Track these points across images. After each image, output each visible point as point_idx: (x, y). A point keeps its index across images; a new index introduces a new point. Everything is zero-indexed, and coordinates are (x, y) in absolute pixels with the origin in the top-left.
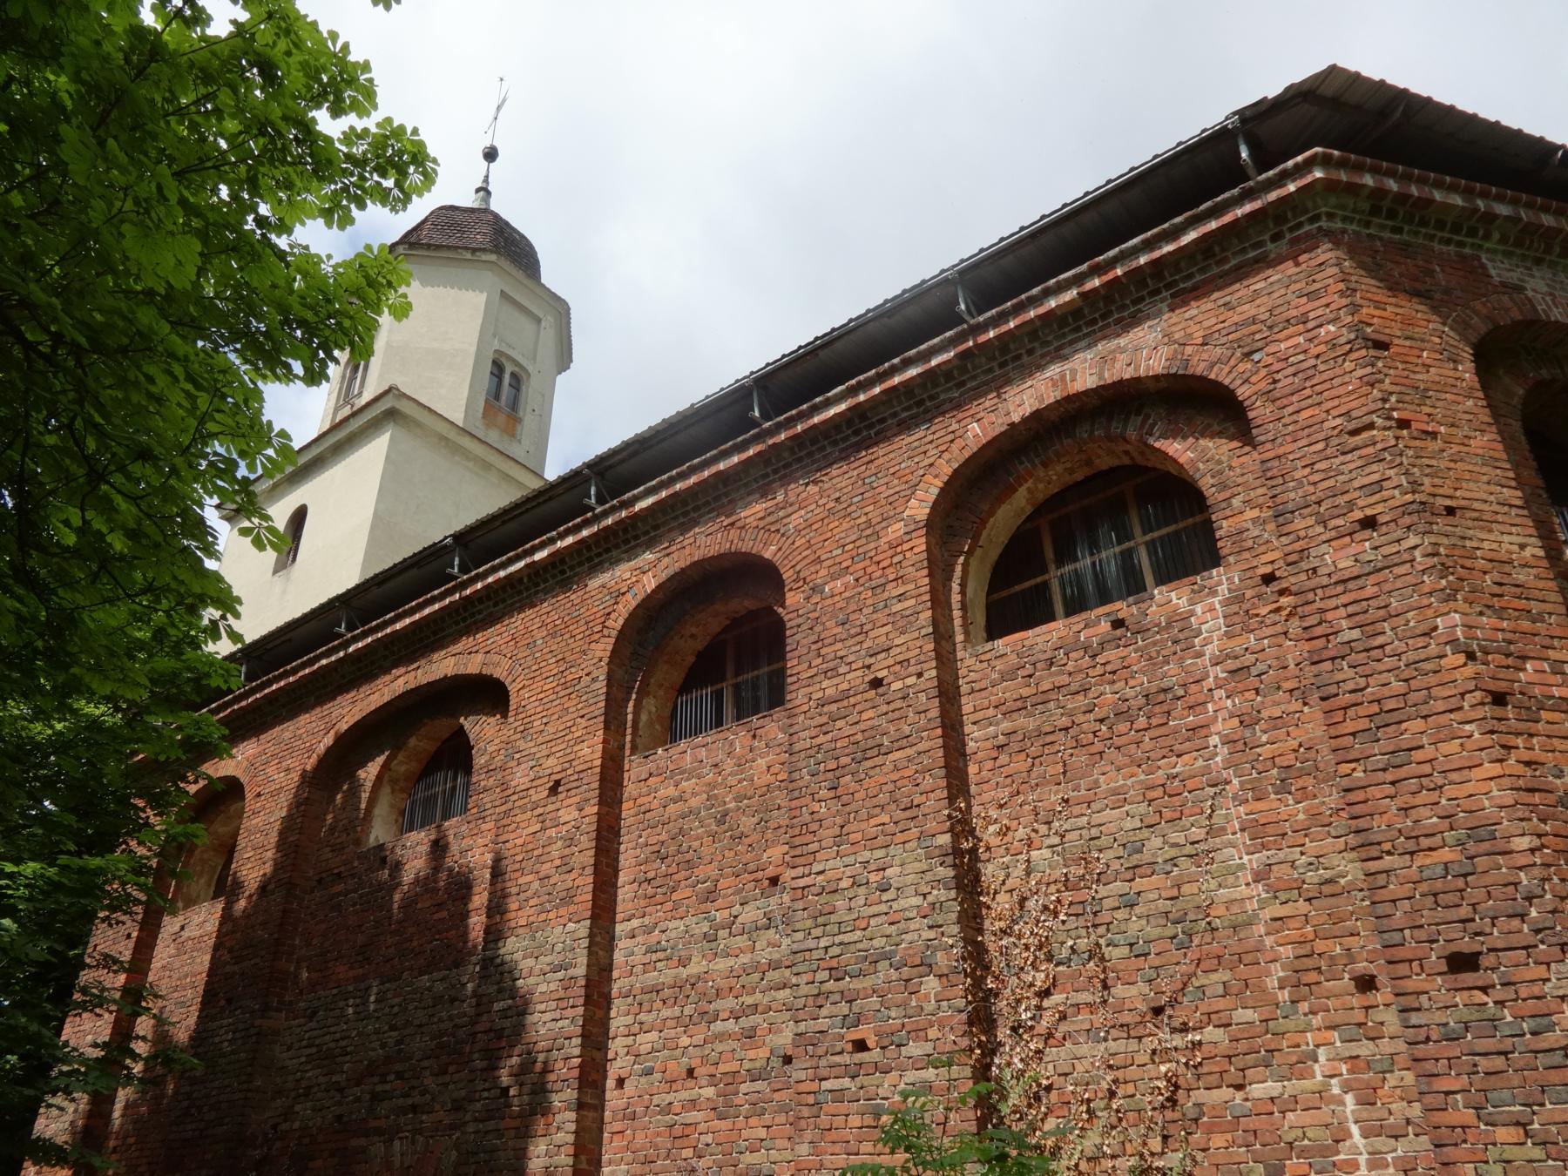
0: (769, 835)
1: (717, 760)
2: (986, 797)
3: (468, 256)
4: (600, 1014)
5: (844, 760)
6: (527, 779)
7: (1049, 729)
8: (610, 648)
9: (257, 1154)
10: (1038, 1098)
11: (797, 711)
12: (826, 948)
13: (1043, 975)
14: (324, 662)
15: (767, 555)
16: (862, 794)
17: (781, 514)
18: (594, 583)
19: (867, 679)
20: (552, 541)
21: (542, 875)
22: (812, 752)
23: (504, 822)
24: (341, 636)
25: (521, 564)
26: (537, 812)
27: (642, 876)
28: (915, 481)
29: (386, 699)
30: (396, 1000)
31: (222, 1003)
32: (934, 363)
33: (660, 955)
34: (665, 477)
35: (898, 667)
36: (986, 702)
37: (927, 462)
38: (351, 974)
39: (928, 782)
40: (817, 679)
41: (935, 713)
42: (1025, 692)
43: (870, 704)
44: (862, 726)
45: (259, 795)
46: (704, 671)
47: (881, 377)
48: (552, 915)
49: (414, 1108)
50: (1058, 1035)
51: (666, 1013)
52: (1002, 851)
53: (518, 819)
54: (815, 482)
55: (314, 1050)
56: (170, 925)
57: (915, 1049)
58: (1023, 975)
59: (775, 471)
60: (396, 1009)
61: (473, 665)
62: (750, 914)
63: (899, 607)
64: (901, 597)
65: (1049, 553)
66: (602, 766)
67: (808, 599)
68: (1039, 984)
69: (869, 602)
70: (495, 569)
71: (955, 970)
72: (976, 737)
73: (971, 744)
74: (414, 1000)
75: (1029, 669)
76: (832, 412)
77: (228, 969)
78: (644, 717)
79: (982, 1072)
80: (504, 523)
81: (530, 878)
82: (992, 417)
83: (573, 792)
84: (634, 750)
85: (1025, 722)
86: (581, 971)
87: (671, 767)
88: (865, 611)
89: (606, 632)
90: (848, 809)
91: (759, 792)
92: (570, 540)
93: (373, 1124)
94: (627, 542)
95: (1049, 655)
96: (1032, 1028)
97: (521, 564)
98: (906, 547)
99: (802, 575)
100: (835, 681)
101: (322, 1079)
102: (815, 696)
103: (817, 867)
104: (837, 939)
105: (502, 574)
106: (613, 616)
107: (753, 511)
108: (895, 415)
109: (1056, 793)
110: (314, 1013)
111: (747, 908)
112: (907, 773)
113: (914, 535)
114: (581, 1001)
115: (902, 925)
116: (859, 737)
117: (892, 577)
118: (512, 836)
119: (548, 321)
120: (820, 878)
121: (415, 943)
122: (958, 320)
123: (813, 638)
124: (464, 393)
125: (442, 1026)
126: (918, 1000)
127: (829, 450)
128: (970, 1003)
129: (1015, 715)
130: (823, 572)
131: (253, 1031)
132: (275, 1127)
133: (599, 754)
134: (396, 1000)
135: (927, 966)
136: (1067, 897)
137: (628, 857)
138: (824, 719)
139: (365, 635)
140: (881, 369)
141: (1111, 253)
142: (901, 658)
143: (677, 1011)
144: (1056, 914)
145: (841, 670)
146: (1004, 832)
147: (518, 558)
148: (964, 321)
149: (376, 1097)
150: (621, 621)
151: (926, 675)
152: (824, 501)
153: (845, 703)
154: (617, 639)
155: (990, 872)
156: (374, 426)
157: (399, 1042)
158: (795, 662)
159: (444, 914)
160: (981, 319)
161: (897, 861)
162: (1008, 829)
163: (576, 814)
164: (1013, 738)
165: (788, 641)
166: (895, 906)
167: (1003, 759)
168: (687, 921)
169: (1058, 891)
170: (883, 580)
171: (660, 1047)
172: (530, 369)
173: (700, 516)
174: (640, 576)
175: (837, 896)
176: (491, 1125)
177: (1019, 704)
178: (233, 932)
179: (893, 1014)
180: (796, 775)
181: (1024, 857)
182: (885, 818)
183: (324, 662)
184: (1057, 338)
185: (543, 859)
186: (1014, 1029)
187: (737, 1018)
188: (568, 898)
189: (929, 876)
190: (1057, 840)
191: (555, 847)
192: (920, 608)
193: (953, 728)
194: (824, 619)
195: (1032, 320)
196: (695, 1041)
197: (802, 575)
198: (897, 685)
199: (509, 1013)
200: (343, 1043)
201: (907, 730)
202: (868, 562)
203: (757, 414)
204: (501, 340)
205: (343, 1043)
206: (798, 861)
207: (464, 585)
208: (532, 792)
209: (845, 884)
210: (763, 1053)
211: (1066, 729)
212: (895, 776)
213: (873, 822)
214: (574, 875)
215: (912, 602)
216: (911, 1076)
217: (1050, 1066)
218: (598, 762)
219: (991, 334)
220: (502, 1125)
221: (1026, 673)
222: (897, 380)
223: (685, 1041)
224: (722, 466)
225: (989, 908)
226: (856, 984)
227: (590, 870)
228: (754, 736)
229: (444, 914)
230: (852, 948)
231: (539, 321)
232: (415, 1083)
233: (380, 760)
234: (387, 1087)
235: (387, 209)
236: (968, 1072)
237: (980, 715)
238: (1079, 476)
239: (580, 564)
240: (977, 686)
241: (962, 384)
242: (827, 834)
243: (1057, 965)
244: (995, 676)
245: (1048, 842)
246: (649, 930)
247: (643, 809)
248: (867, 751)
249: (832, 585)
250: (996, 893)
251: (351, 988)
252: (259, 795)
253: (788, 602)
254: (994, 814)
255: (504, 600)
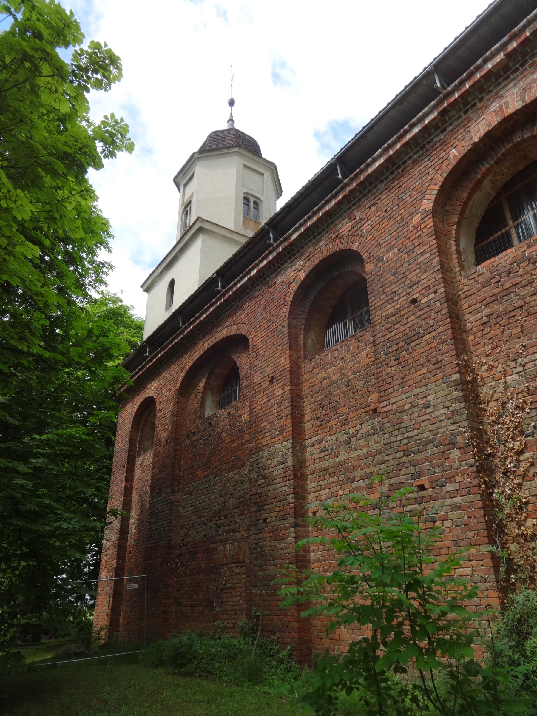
0: (371, 388)
1: (343, 356)
2: (479, 352)
3: (226, 151)
4: (301, 483)
5: (401, 344)
6: (259, 379)
7: (511, 309)
8: (288, 310)
9: (177, 552)
10: (521, 509)
11: (376, 323)
12: (401, 440)
13: (518, 443)
14: (176, 341)
15: (354, 248)
16: (411, 360)
17: (359, 226)
18: (279, 280)
19: (409, 300)
20: (257, 265)
21: (270, 421)
22: (385, 343)
23: (253, 399)
24: (181, 327)
25: (246, 279)
26: (265, 393)
27: (315, 417)
28: (424, 190)
29: (202, 352)
30: (221, 484)
31: (157, 491)
32: (427, 121)
33: (326, 453)
34: (302, 221)
35: (424, 291)
36: (475, 301)
37: (429, 178)
38: (203, 474)
39: (445, 347)
40: (384, 305)
41: (445, 311)
42: (496, 291)
43: (411, 313)
44: (408, 325)
45: (161, 402)
46: (336, 315)
47: (399, 138)
48: (276, 439)
49: (232, 530)
50: (530, 475)
51: (332, 480)
52: (490, 379)
53: (258, 397)
54: (374, 205)
55: (193, 508)
56: (139, 460)
57: (449, 487)
58: (507, 444)
59: (354, 205)
60: (221, 488)
61: (233, 331)
62: (365, 428)
63: (422, 259)
64: (422, 254)
65: (508, 215)
66: (290, 367)
67: (375, 266)
68: (516, 448)
69: (406, 260)
70: (235, 284)
71: (467, 445)
72: (471, 320)
73: (468, 325)
74: (227, 483)
75: (497, 278)
76: (377, 164)
77: (158, 476)
78: (309, 342)
79: (487, 497)
80: (237, 262)
81: (265, 423)
82: (463, 143)
83: (279, 381)
84: (305, 357)
85: (498, 307)
86: (290, 464)
87: (322, 363)
88: (405, 265)
89: (286, 303)
90: (405, 369)
91: (363, 368)
92: (265, 263)
93: (218, 538)
94: (290, 258)
95: (508, 267)
96: (515, 471)
97: (246, 279)
98: (422, 226)
99: (372, 254)
100: (393, 305)
101: (198, 520)
102: (384, 315)
103: (392, 401)
104: (405, 436)
105: (239, 285)
106: (288, 295)
107: (345, 227)
108: (410, 158)
109: (518, 343)
110: (192, 492)
111: (363, 426)
112: (433, 345)
113: (426, 219)
114: (292, 477)
115: (438, 424)
116: (408, 331)
117: (416, 244)
118: (256, 405)
119: (267, 175)
120: (395, 406)
121: (225, 459)
122: (437, 92)
123: (380, 285)
124: (233, 215)
125: (240, 494)
126: (449, 462)
127: (379, 186)
128: (477, 461)
129: (491, 305)
130: (382, 250)
131: (169, 501)
132: (183, 540)
133: (288, 362)
134: (221, 484)
135: (453, 444)
136: (529, 399)
137: (308, 408)
138: (389, 325)
139: (189, 325)
140: (399, 134)
141: (521, 24)
142: (425, 285)
143: (336, 478)
144: (523, 409)
145: (395, 299)
146: (490, 369)
147: (244, 276)
148: (441, 93)
149: (218, 527)
150: (292, 297)
151: (439, 292)
152: (379, 213)
153: (399, 315)
154: (291, 305)
155: (484, 391)
156: (194, 236)
157: (224, 502)
158: (373, 299)
159: (235, 444)
160: (449, 89)
161: (432, 392)
162: (493, 367)
163: (281, 391)
164: (492, 317)
165: (368, 289)
166: (433, 415)
167: (487, 330)
168: (336, 435)
169: (524, 397)
170: (412, 247)
171: (329, 496)
172: (262, 198)
173: (322, 237)
174: (297, 272)
175: (404, 414)
176: (260, 536)
177: (493, 298)
178: (158, 461)
179: (437, 471)
180: (378, 356)
181: (503, 380)
182: (424, 370)
183: (176, 341)
184: (495, 87)
185: (270, 414)
186: (504, 473)
187: (363, 480)
188: (282, 431)
189: (449, 397)
190: (521, 369)
191: (274, 408)
192: (433, 256)
193: (458, 317)
194: (385, 274)
195: (479, 81)
196: (345, 492)
197: (372, 254)
198: (425, 300)
199: (263, 485)
200: (203, 504)
201: (431, 322)
202: (404, 239)
203: (340, 176)
204: (246, 188)
205: (203, 504)
206: (383, 398)
207: (224, 294)
208: (262, 384)
209: (407, 407)
210: (378, 495)
211: (521, 307)
212: (427, 348)
213: (418, 373)
214: (283, 420)
215: (429, 254)
216: (449, 501)
217: (527, 492)
218: (288, 366)
219: (457, 95)
220: (265, 535)
221: (495, 280)
222: (408, 137)
223: (341, 492)
224: (327, 208)
225: (485, 410)
226: (417, 457)
227: (289, 417)
228: (359, 341)
229: (235, 444)
230: (414, 439)
231: (263, 175)
232: (232, 519)
233: (204, 380)
234: (221, 522)
235: (103, 90)
236: (479, 497)
237: (472, 308)
238: (521, 167)
239: (272, 273)
240: (469, 293)
241: (445, 129)
242: (396, 383)
243: (526, 437)
244: (478, 286)
245: (516, 370)
246: (320, 442)
247: (312, 385)
248: (412, 337)
249: (387, 256)
250: (489, 402)
251: (204, 481)
252: (161, 402)
253: (366, 270)
254: (484, 360)
255: (242, 298)
